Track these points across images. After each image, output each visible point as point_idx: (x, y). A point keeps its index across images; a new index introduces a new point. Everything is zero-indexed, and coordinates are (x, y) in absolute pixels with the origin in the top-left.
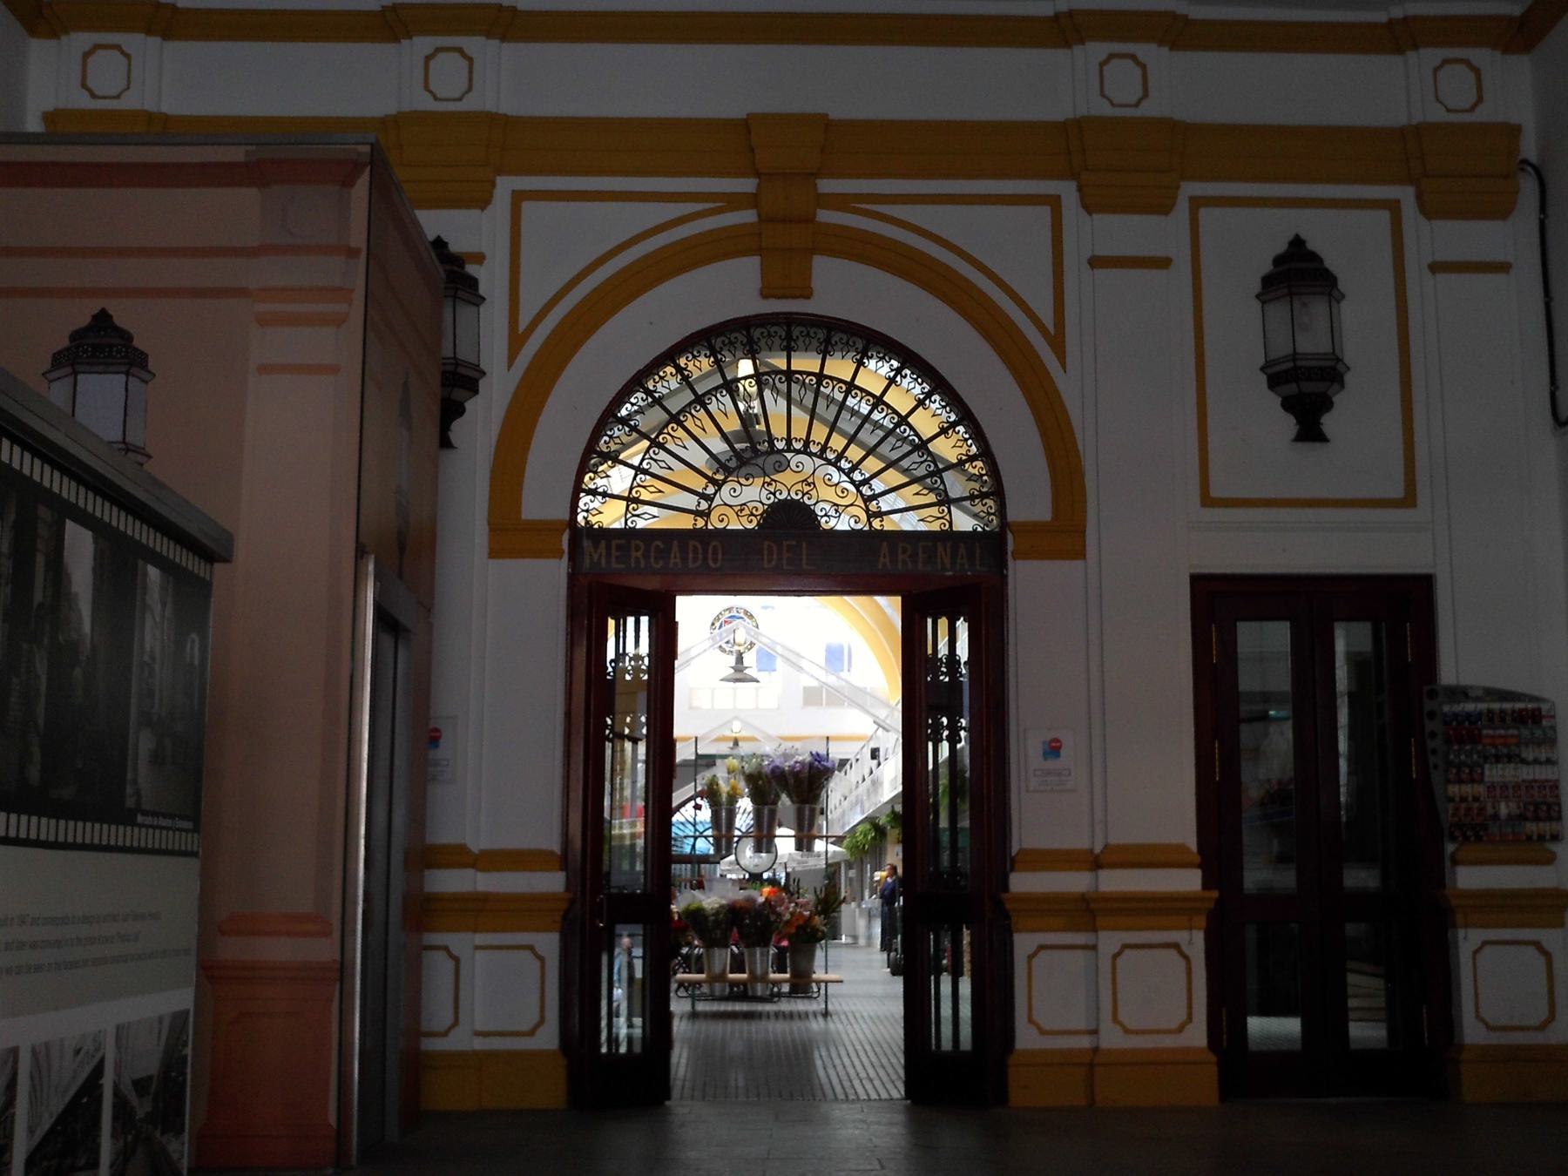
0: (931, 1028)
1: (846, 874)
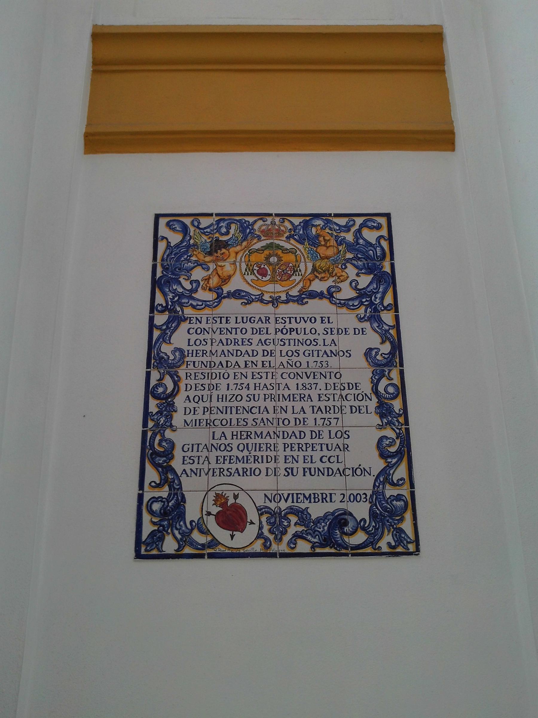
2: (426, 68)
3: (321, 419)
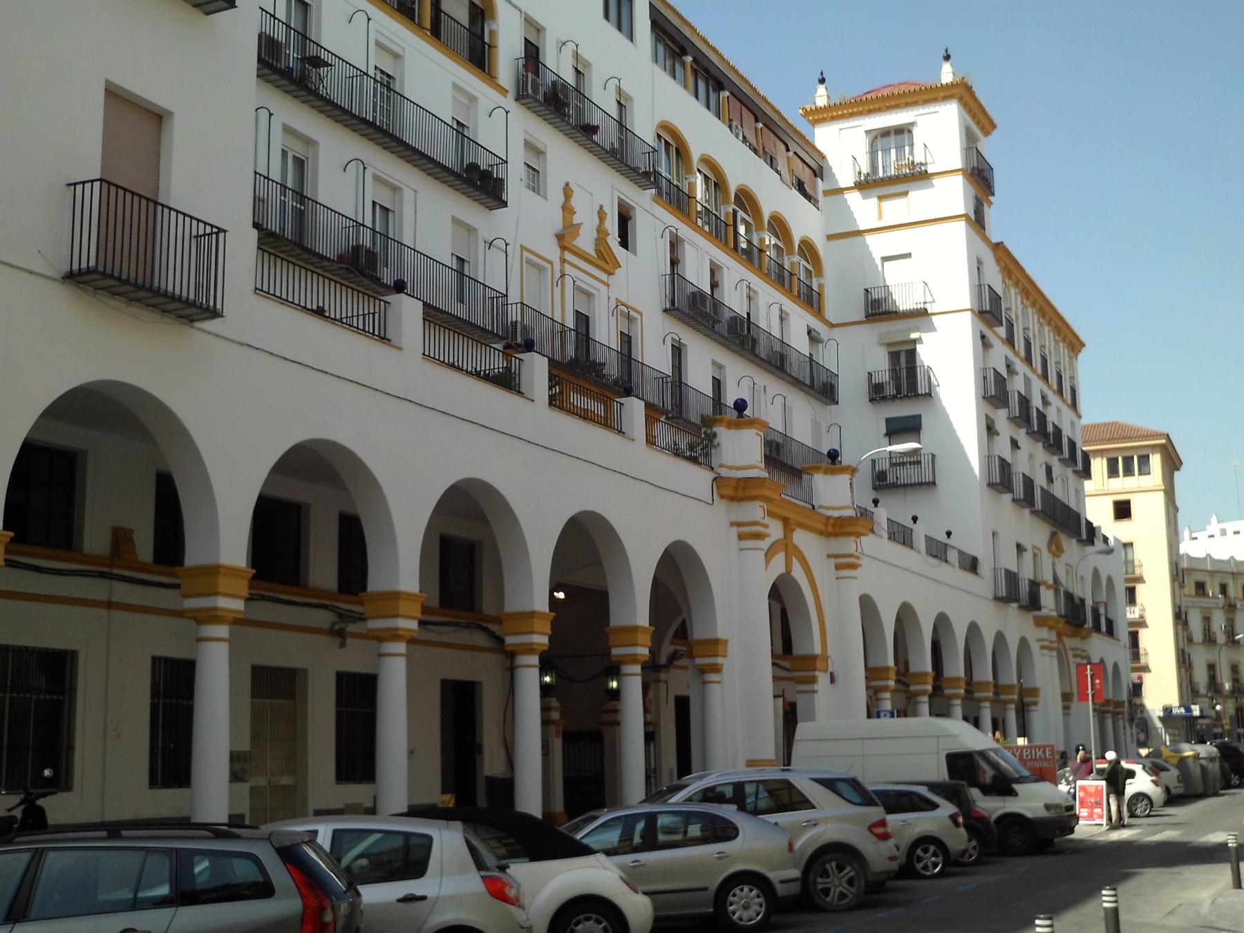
0: (579, 816)
2: (353, 614)
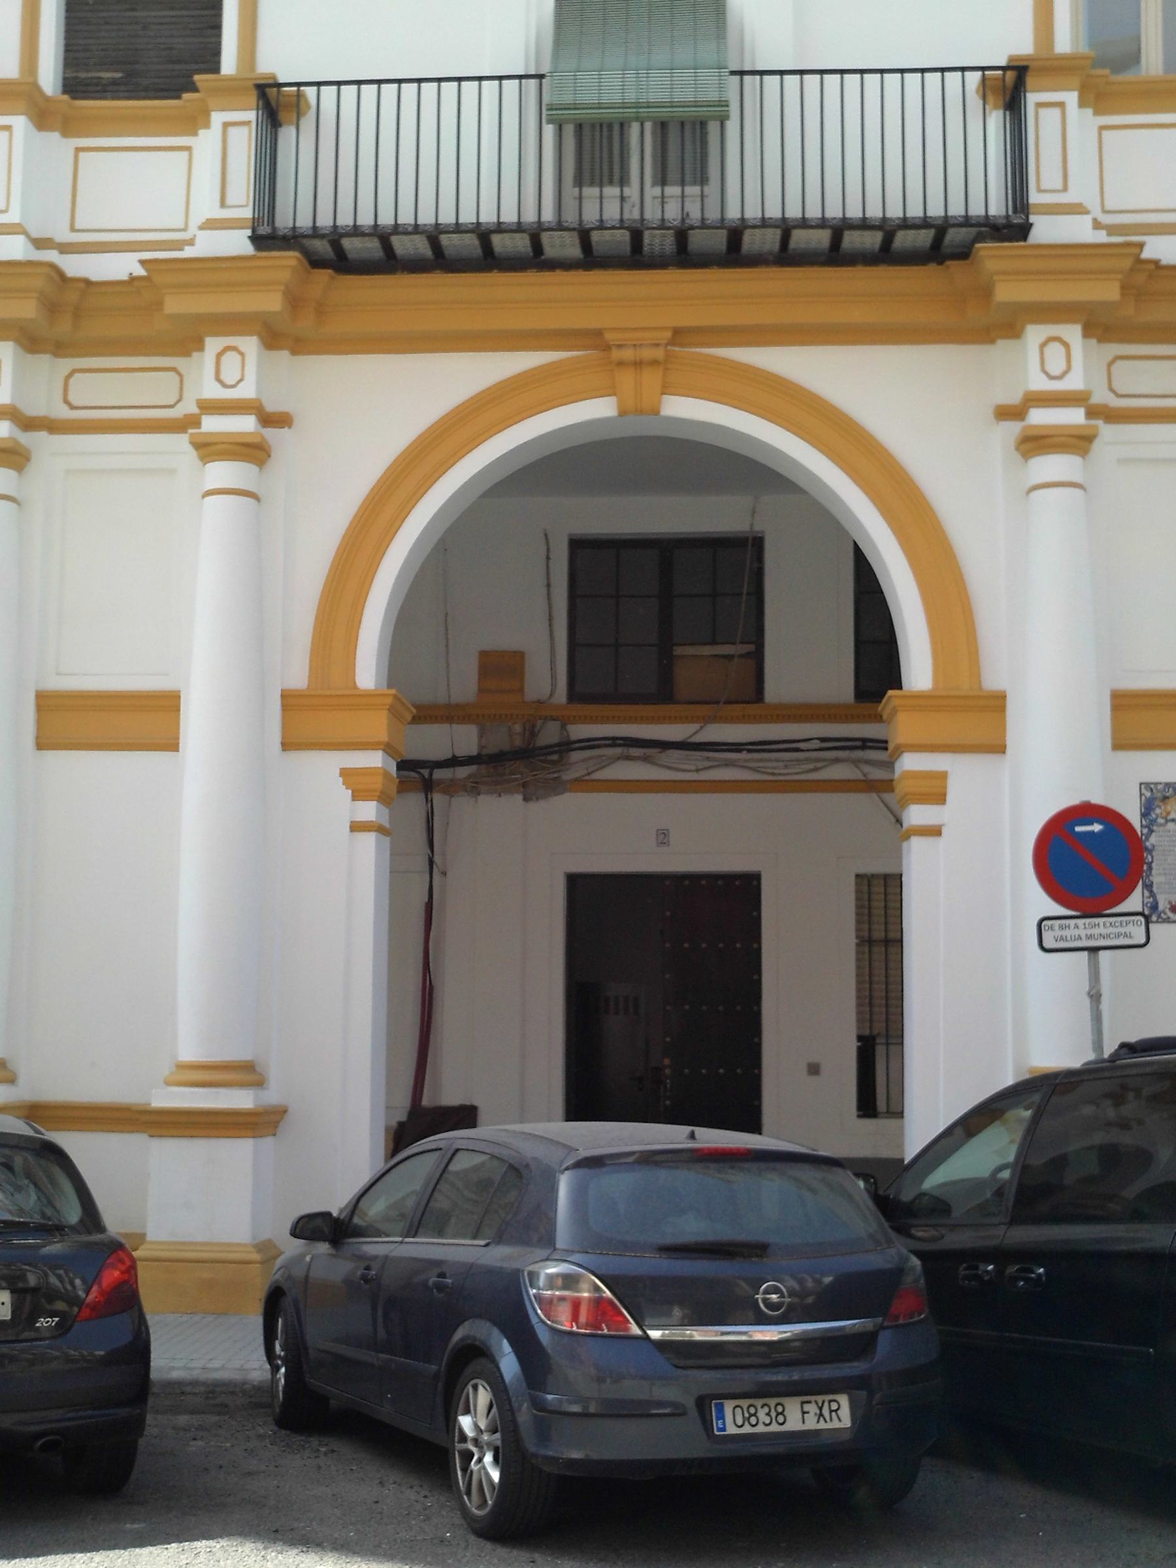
1: (562, 1299)
3: (818, 1422)
